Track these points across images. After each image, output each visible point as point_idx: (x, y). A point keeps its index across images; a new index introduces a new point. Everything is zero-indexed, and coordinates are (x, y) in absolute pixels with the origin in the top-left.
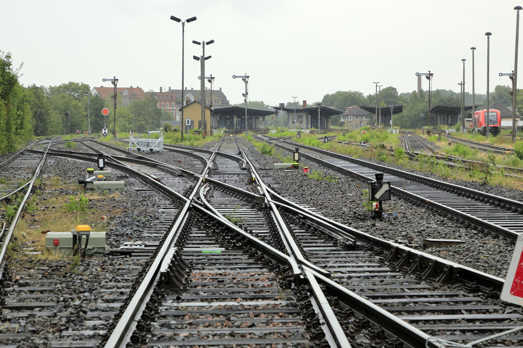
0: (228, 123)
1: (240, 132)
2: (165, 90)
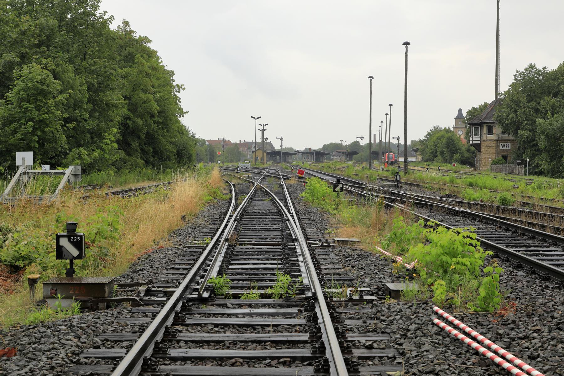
0: (274, 158)
1: (278, 163)
2: (242, 141)
